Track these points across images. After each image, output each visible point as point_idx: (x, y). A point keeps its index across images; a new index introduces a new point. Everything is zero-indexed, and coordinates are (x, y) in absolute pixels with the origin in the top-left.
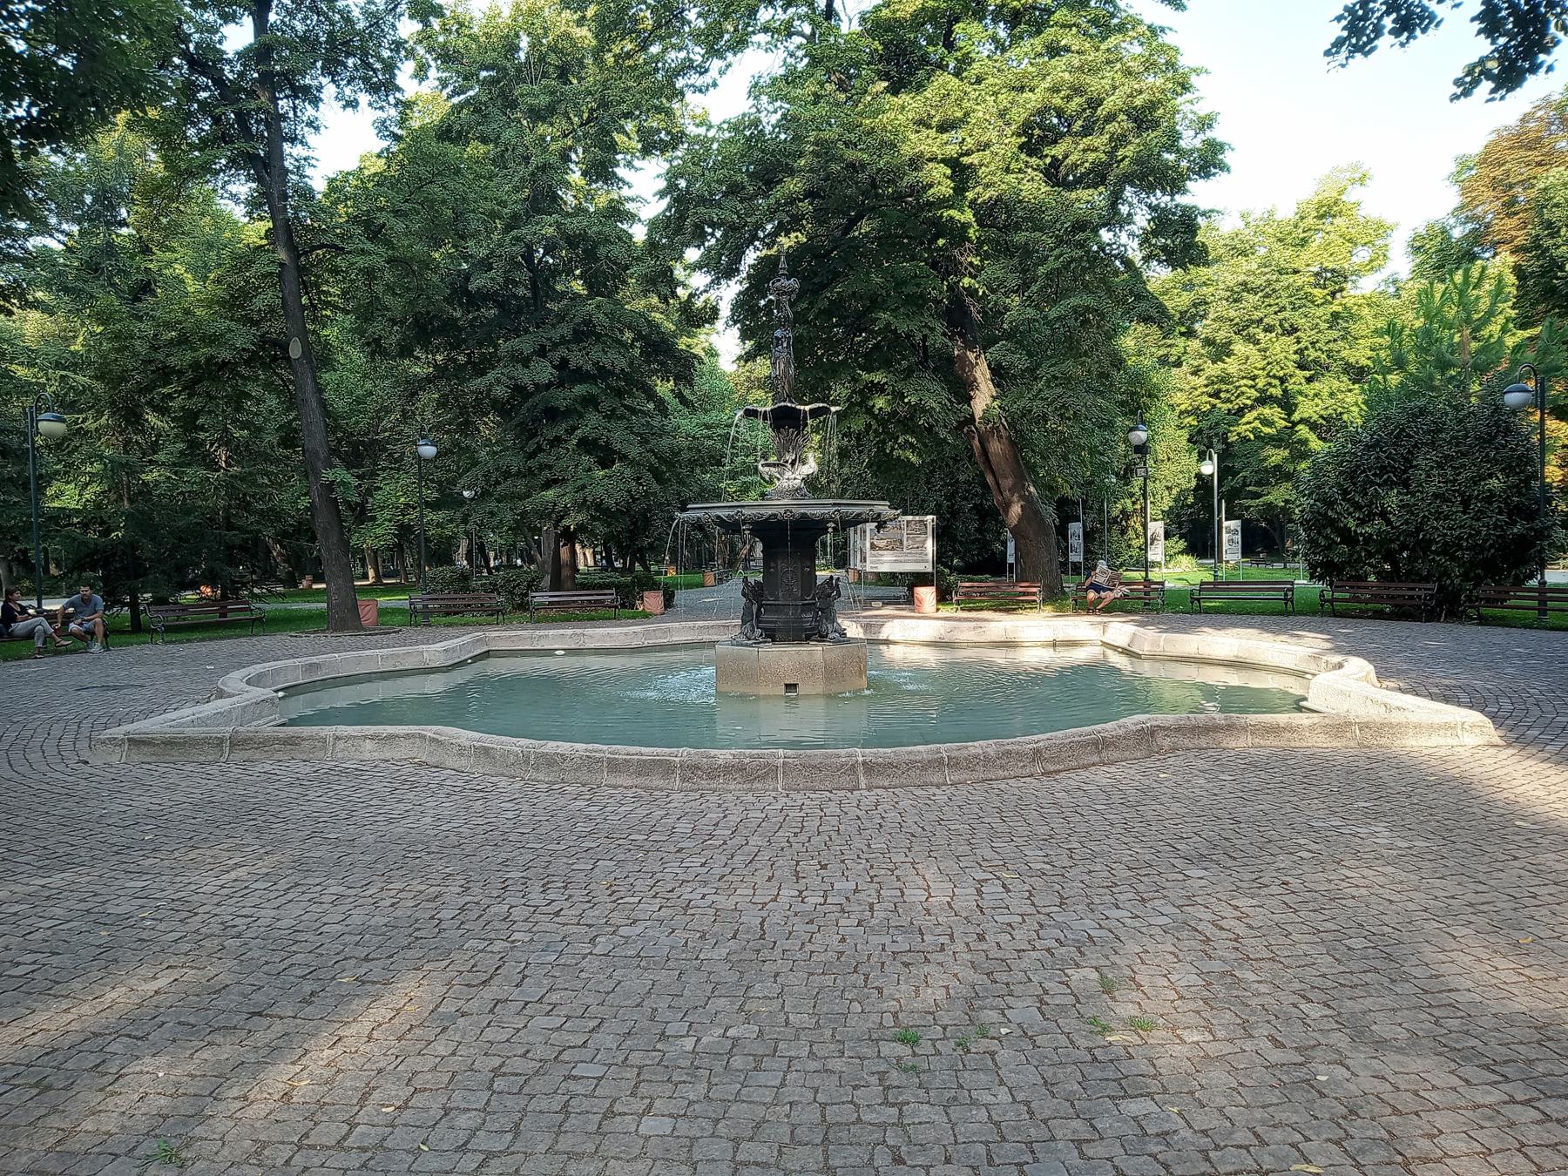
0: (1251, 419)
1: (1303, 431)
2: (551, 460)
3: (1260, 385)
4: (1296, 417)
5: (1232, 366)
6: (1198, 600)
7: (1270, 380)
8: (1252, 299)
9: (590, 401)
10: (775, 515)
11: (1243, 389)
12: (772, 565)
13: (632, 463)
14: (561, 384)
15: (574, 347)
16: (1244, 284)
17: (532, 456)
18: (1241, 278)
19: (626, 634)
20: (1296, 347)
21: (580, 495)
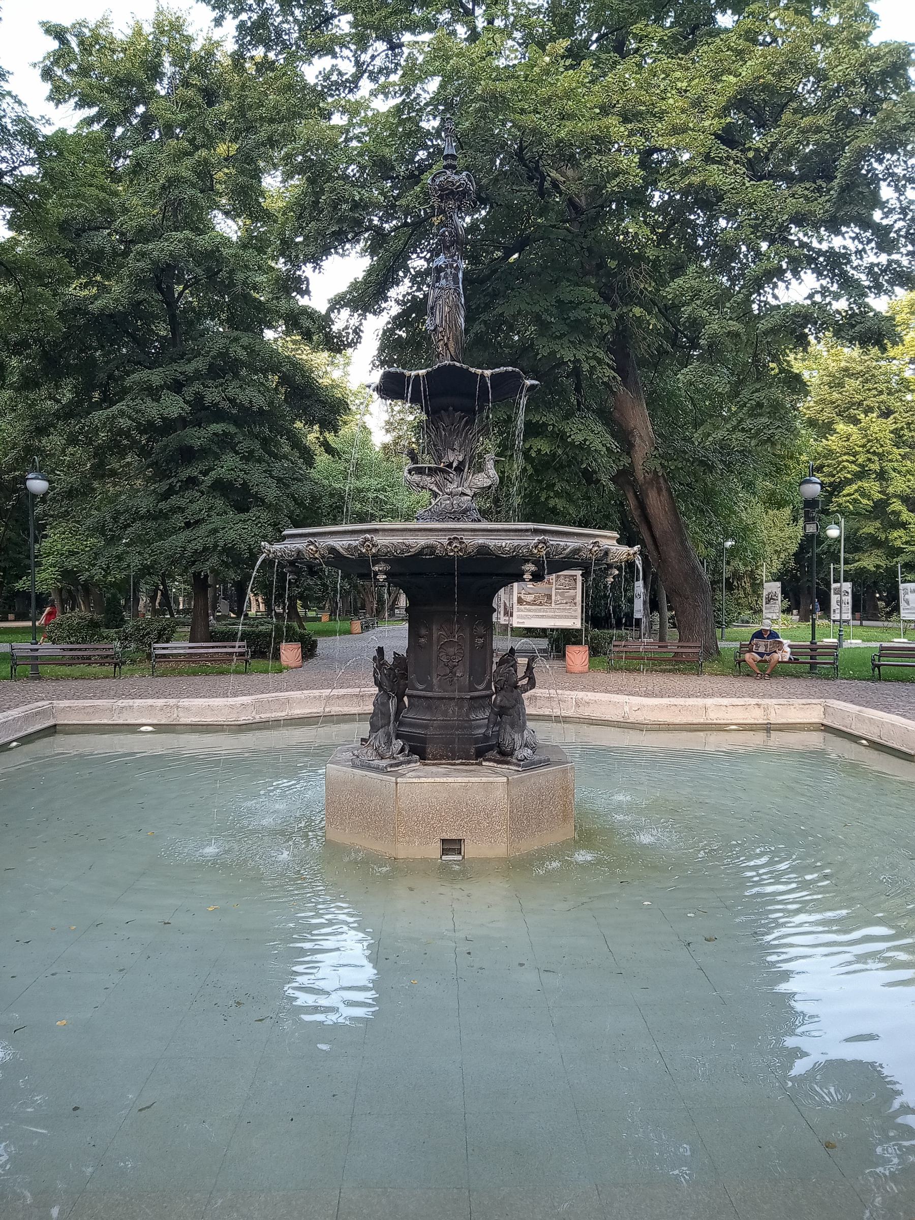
0: (852, 491)
1: (897, 505)
2: (182, 502)
4: (891, 490)
5: (833, 442)
6: (878, 666)
7: (869, 456)
8: (852, 384)
9: (225, 442)
10: (431, 548)
11: (845, 464)
12: (423, 632)
15: (210, 383)
16: (846, 370)
17: (165, 496)
18: (843, 364)
19: (232, 707)
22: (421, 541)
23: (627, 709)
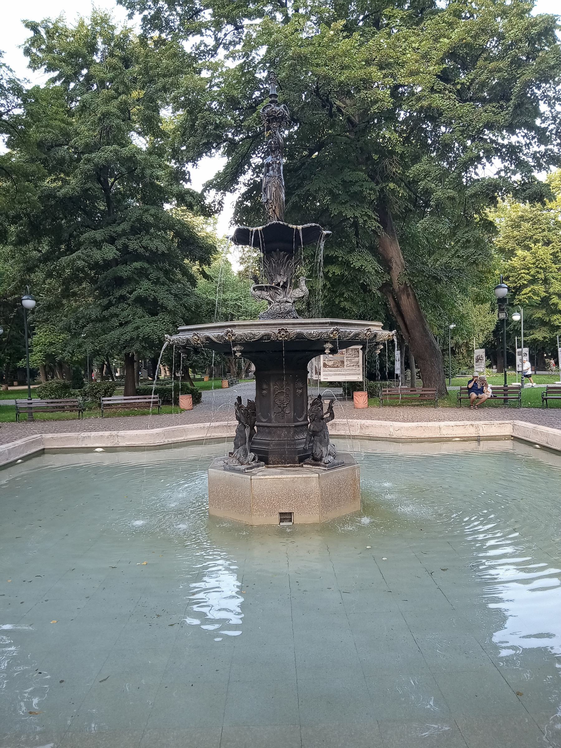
0: (527, 291)
3: (532, 273)
4: (551, 290)
5: (515, 262)
6: (546, 399)
8: (527, 225)
9: (142, 273)
10: (268, 336)
11: (523, 275)
12: (265, 386)
13: (170, 312)
14: (125, 263)
15: (132, 237)
16: (522, 217)
17: (107, 307)
18: (520, 213)
20: (552, 251)
21: (135, 333)
22: (262, 331)
23: (391, 430)
